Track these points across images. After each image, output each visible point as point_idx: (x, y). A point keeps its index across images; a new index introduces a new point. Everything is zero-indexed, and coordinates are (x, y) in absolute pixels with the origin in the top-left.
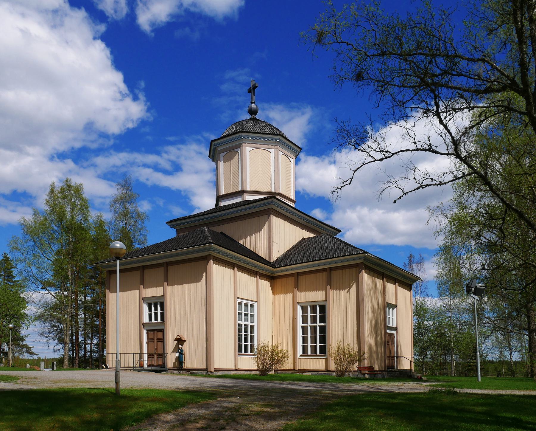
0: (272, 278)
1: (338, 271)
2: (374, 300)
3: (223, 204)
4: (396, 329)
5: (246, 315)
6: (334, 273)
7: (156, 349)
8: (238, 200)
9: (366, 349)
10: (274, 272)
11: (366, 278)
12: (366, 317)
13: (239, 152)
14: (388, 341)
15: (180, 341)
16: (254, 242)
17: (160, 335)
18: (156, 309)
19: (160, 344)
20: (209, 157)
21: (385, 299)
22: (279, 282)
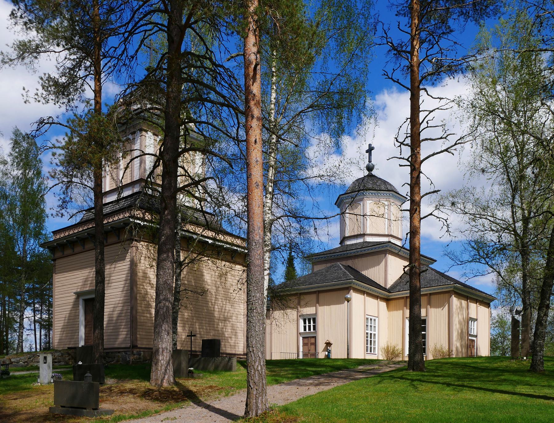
0: (387, 300)
1: (435, 296)
2: (460, 316)
3: (348, 243)
4: (476, 336)
5: (371, 326)
6: (433, 297)
7: (309, 350)
8: (360, 240)
9: (454, 349)
10: (389, 296)
11: (455, 301)
12: (454, 328)
13: (362, 204)
14: (470, 344)
15: (328, 344)
16: (373, 273)
17: (313, 340)
18: (309, 323)
19: (313, 347)
20: (335, 204)
21: (468, 314)
22: (392, 303)
